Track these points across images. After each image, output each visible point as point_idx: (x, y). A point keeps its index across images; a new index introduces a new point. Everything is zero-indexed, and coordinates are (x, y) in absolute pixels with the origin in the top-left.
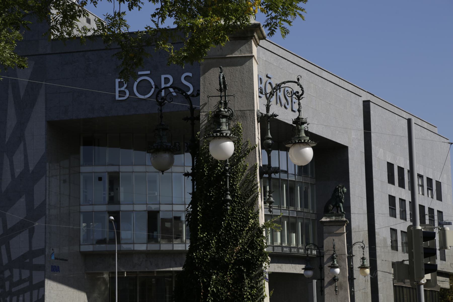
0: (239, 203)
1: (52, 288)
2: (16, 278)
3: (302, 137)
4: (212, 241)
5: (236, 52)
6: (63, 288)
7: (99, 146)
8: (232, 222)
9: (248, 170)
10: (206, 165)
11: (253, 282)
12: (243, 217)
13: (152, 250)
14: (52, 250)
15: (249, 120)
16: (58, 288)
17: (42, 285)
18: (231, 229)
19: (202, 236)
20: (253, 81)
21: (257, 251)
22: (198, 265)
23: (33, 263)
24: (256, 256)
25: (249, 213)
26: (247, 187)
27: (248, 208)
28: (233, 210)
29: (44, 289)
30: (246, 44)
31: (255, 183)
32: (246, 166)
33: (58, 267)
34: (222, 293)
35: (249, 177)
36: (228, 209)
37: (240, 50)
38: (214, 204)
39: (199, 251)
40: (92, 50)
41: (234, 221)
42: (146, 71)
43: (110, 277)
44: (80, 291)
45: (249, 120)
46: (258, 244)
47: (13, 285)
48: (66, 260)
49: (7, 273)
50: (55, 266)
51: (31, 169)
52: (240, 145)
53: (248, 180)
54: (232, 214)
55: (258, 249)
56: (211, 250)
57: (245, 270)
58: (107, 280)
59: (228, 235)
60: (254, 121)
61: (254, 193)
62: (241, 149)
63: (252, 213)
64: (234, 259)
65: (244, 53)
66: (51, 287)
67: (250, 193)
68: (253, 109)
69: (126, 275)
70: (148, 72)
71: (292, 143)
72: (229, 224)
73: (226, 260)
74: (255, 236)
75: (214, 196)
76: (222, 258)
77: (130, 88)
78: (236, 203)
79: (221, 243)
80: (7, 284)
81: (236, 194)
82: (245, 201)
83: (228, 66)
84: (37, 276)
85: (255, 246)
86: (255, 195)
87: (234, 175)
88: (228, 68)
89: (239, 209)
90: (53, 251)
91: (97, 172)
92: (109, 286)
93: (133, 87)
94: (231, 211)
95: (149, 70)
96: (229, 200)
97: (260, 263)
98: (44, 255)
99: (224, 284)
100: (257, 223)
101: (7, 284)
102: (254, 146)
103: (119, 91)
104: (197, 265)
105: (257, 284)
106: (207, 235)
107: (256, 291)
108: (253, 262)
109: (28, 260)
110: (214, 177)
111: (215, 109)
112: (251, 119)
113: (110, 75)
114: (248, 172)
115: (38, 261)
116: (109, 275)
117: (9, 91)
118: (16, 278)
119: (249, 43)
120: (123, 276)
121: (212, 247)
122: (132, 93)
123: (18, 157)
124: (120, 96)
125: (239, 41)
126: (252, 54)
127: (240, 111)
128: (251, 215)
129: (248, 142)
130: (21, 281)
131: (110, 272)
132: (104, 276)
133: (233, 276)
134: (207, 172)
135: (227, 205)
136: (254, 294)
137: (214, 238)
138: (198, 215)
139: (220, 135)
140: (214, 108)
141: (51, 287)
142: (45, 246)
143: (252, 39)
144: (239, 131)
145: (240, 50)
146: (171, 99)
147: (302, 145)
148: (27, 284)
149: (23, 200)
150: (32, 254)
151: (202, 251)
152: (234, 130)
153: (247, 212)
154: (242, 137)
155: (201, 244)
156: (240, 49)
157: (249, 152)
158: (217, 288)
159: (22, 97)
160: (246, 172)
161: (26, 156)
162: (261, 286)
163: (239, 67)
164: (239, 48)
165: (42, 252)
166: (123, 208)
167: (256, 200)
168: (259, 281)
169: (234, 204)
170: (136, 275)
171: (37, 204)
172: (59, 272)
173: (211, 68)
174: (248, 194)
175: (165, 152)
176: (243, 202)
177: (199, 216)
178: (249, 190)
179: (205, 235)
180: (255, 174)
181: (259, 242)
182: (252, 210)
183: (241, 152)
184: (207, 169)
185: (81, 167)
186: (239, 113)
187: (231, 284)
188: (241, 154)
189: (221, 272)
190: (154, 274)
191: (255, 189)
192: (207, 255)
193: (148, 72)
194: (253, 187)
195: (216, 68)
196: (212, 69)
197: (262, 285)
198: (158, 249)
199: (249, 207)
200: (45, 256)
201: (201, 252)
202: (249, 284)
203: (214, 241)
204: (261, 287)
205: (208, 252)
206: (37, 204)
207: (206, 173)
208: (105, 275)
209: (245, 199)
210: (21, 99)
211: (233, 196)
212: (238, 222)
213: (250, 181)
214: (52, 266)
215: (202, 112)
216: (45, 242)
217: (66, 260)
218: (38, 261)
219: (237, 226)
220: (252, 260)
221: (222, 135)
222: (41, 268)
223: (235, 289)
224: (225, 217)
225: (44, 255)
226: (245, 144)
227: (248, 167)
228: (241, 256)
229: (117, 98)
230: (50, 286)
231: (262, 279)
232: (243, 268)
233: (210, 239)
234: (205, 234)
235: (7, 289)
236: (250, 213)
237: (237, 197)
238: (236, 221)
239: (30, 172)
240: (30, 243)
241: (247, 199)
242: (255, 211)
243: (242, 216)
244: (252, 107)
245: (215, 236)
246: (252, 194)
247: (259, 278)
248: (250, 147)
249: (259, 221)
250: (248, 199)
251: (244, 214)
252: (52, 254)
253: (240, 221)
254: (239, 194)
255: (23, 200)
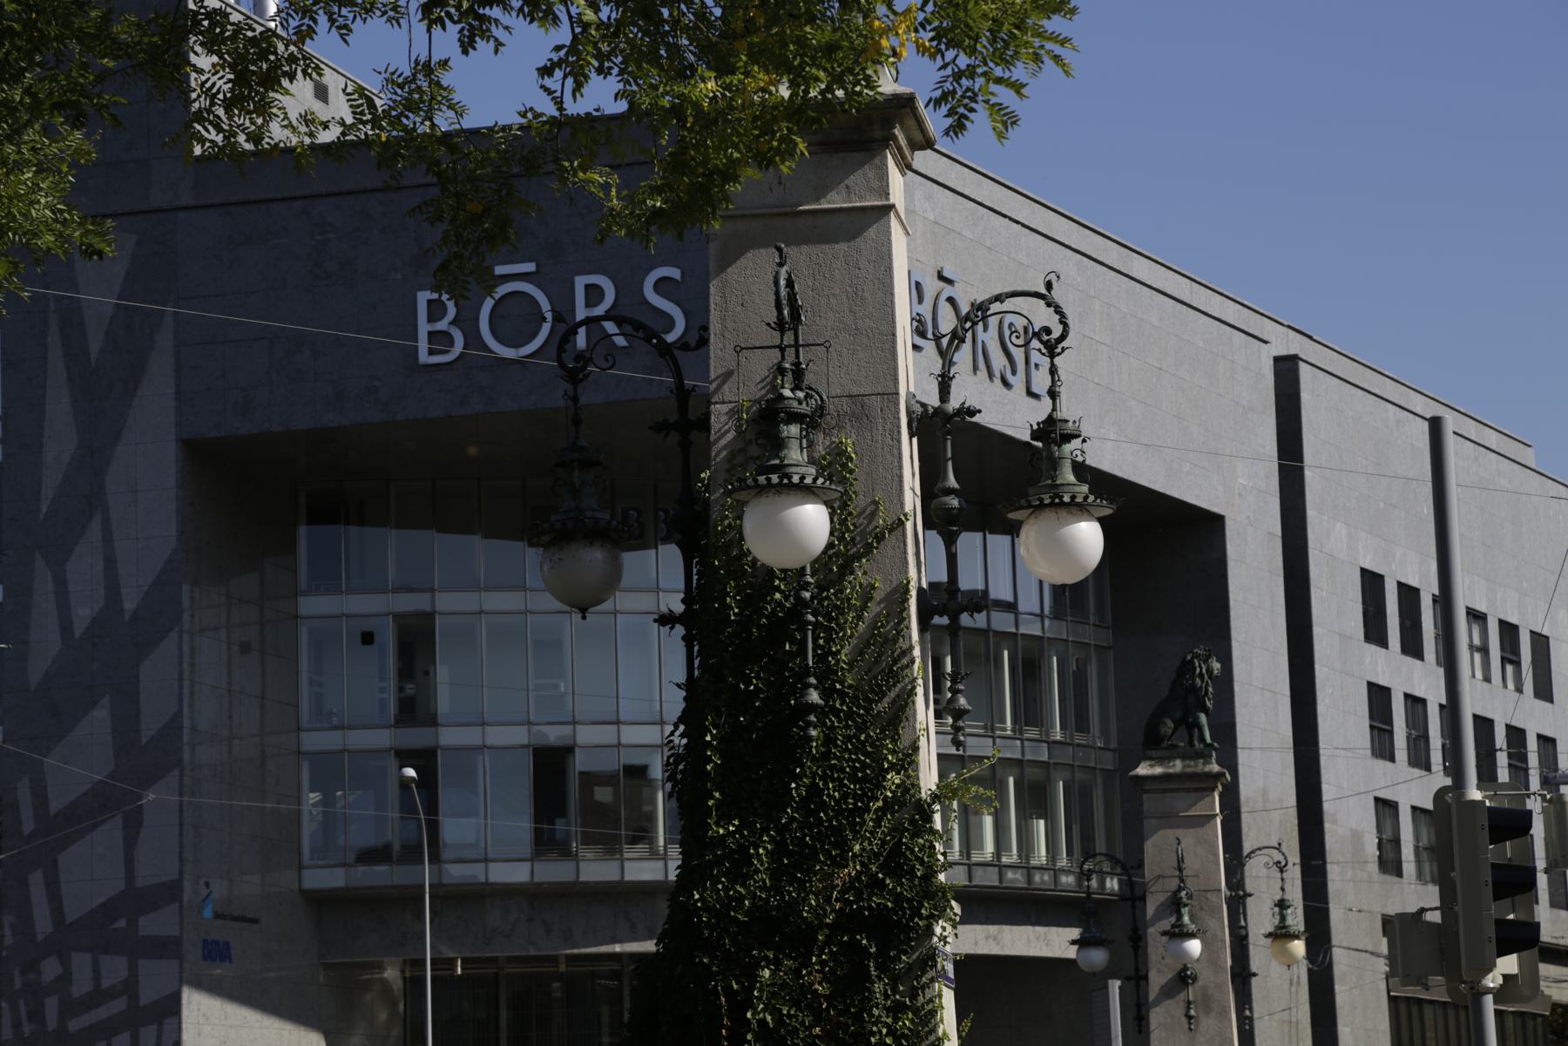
0: (850, 715)
1: (207, 1019)
2: (81, 986)
3: (1063, 485)
4: (757, 849)
5: (833, 195)
6: (245, 1018)
7: (361, 523)
8: (826, 784)
9: (879, 603)
10: (734, 588)
11: (901, 988)
12: (864, 766)
13: (549, 883)
14: (204, 887)
15: (880, 428)
16: (226, 1018)
17: (171, 1008)
18: (824, 806)
19: (721, 831)
20: (892, 295)
21: (912, 881)
22: (711, 934)
23: (140, 933)
24: (909, 901)
25: (885, 752)
26: (877, 662)
27: (880, 733)
28: (829, 740)
29: (180, 1022)
30: (866, 167)
31: (905, 647)
32: (873, 587)
33: (227, 944)
34: (796, 1030)
35: (882, 626)
36: (811, 739)
37: (847, 187)
38: (762, 722)
39: (714, 885)
40: (335, 194)
41: (833, 780)
42: (522, 261)
43: (404, 979)
44: (302, 1028)
45: (880, 428)
46: (917, 858)
47: (70, 1008)
48: (254, 921)
49: (50, 969)
50: (217, 943)
51: (129, 605)
52: (850, 514)
53: (880, 634)
54: (826, 756)
55: (917, 877)
56: (755, 882)
57: (873, 950)
58: (395, 987)
59: (811, 829)
60: (896, 433)
61: (899, 682)
62: (852, 528)
63: (894, 752)
64: (833, 910)
65: (861, 198)
66: (204, 1015)
67: (887, 681)
68: (893, 391)
69: (462, 969)
70: (530, 267)
71: (1030, 506)
72: (815, 792)
73: (805, 915)
74: (907, 830)
75: (763, 692)
76: (793, 907)
77: (466, 321)
78: (838, 717)
79: (790, 854)
80: (52, 1005)
81: (838, 686)
82: (868, 710)
83: (807, 244)
84: (153, 978)
85: (904, 863)
86: (904, 688)
87: (830, 619)
88: (805, 248)
89: (848, 739)
90: (208, 888)
91: (355, 616)
92: (401, 1007)
93: (477, 319)
94: (822, 745)
95: (530, 261)
96: (813, 708)
97: (925, 922)
98: (177, 904)
99: (801, 996)
100: (913, 785)
101: (52, 1005)
102: (900, 520)
103: (430, 333)
104: (706, 933)
105: (914, 997)
106: (739, 830)
107: (912, 1021)
108: (900, 920)
109: (122, 923)
110: (759, 627)
111: (763, 392)
112: (888, 426)
113: (399, 276)
114: (878, 609)
115: (156, 924)
116: (403, 972)
117: (49, 339)
118: (81, 986)
119: (877, 161)
120: (449, 972)
121: (757, 871)
122: (473, 338)
123: (84, 567)
124: (431, 352)
125: (842, 154)
126: (888, 199)
127: (850, 396)
128: (890, 758)
129: (876, 503)
130: (98, 996)
131: (405, 961)
132: (385, 975)
133: (833, 971)
134: (736, 610)
135: (809, 724)
136: (906, 1032)
137: (765, 838)
138: (709, 760)
139: (781, 481)
140: (759, 387)
141: (204, 1015)
142: (181, 873)
143: (887, 147)
144: (844, 466)
145: (847, 187)
146: (609, 358)
147: (1063, 513)
148: (120, 1004)
149: (101, 714)
150: (137, 900)
151: (723, 883)
152: (830, 464)
153: (878, 748)
154: (858, 486)
155: (718, 862)
156: (846, 182)
157: (880, 538)
158: (775, 1012)
159: (93, 360)
160: (874, 608)
161: (110, 562)
162: (928, 1004)
163: (843, 246)
164: (842, 181)
165: (170, 892)
166: (449, 737)
167: (907, 704)
168: (923, 988)
169: (830, 720)
170: (495, 970)
171: (150, 726)
172: (231, 961)
173: (747, 251)
174: (880, 686)
175: (591, 544)
176: (862, 711)
177: (712, 761)
178: (883, 670)
179: (731, 828)
180: (904, 615)
181: (920, 850)
182: (894, 741)
183: (853, 539)
184: (735, 598)
185: (302, 598)
186: (845, 405)
187: (824, 996)
188: (855, 545)
189: (789, 957)
190: (557, 967)
191: (902, 669)
192: (741, 899)
193: (530, 267)
194: (895, 661)
195: (762, 251)
196: (749, 255)
197: (932, 1001)
198: (570, 877)
199: (883, 731)
200: (181, 907)
201: (720, 886)
202: (886, 997)
203: (765, 848)
204: (931, 1006)
205: (744, 885)
206: (150, 726)
207: (735, 614)
208: (389, 971)
209: (870, 701)
210: (93, 365)
211: (826, 693)
212: (846, 782)
213: (886, 641)
214: (205, 942)
215: (716, 403)
216: (181, 860)
217: (254, 921)
218: (156, 924)
219: (845, 797)
220: (897, 914)
221: (786, 481)
222: (167, 948)
223: (840, 1013)
224: (802, 766)
225: (177, 904)
226: (868, 512)
227: (878, 591)
228: (859, 898)
229: (424, 357)
230: (199, 1010)
231: (932, 980)
232: (864, 942)
233: (751, 844)
234: (734, 825)
235: (52, 1024)
236: (888, 749)
237: (842, 694)
238: (840, 780)
239: (127, 616)
240: (129, 862)
241: (877, 702)
242: (904, 742)
243: (858, 760)
244: (892, 386)
245: (766, 830)
246: (894, 685)
247: (921, 977)
248: (884, 521)
249: (918, 779)
250: (880, 700)
251: (867, 754)
252: (204, 900)
253: (855, 780)
254: (850, 687)
255: (101, 714)
